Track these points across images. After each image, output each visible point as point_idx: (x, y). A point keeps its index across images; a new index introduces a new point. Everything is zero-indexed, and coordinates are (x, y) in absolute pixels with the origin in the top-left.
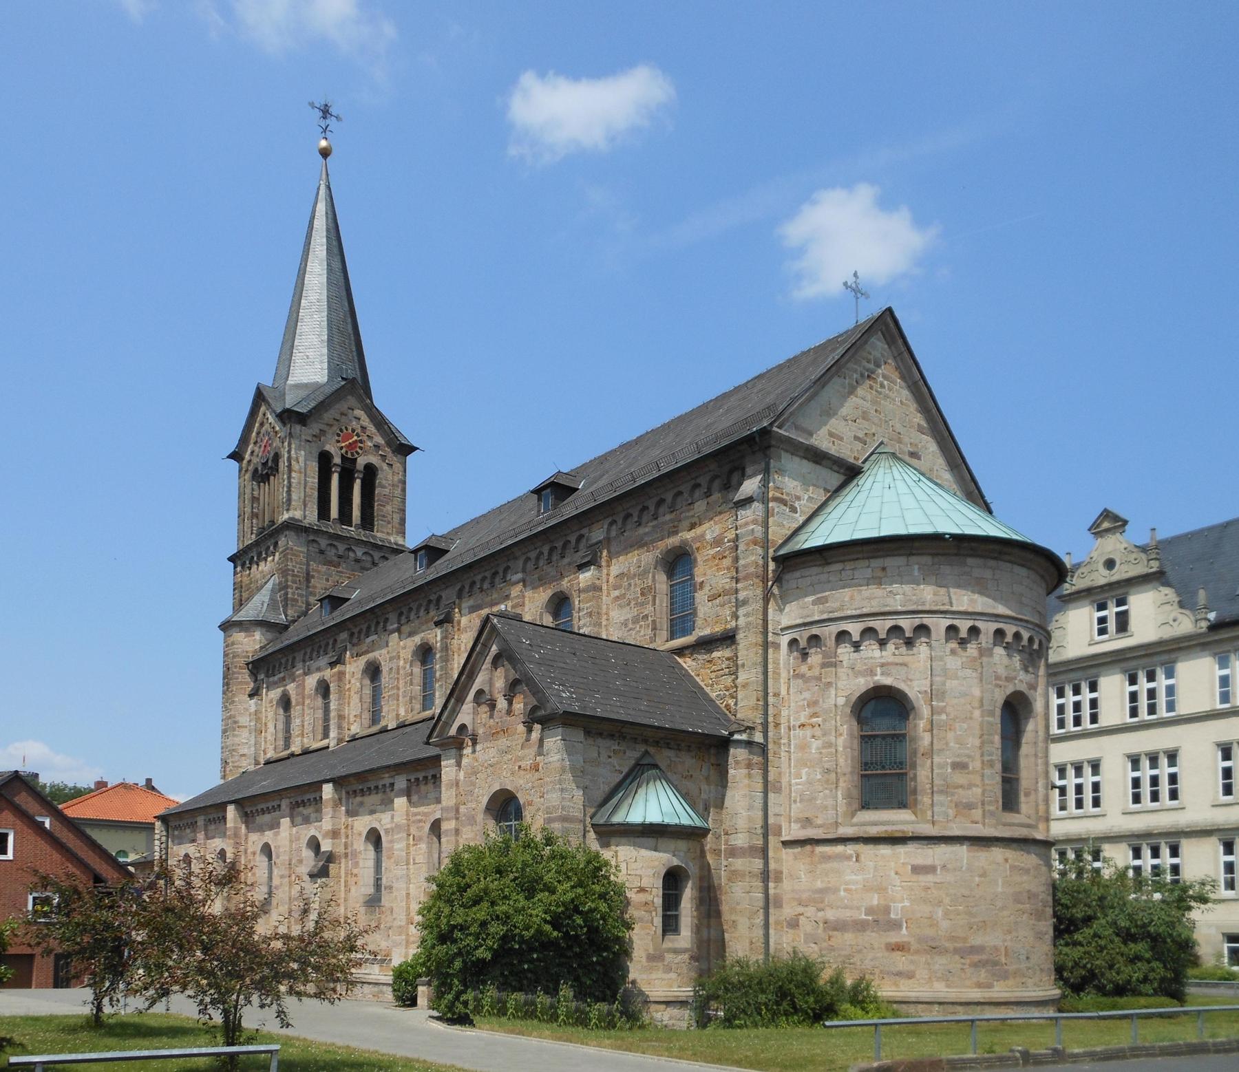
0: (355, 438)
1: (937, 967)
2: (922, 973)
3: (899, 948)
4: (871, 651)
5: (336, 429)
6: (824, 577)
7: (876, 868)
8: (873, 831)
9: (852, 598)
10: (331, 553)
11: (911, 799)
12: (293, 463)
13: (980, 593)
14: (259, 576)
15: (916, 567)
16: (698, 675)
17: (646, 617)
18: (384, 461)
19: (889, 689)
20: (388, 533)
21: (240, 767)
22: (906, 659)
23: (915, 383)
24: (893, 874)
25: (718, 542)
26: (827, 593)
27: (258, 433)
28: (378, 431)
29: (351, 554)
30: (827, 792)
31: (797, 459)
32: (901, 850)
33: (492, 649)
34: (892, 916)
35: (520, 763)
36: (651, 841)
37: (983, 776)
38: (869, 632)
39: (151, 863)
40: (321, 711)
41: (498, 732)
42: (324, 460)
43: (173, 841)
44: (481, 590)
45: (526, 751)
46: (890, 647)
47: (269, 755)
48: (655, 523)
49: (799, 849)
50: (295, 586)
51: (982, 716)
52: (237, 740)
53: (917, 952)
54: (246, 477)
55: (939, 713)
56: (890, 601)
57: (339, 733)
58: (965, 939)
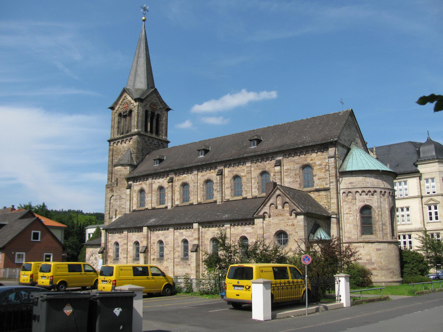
1: (383, 273)
2: (379, 275)
4: (364, 196)
7: (368, 250)
8: (367, 240)
10: (148, 142)
11: (374, 232)
12: (139, 114)
14: (121, 148)
17: (297, 181)
21: (122, 212)
23: (356, 126)
24: (372, 251)
25: (320, 165)
27: (122, 102)
29: (153, 142)
30: (355, 230)
31: (340, 147)
35: (287, 224)
40: (159, 196)
41: (278, 215)
47: (134, 208)
50: (139, 153)
53: (378, 270)
56: (367, 185)
58: (388, 266)
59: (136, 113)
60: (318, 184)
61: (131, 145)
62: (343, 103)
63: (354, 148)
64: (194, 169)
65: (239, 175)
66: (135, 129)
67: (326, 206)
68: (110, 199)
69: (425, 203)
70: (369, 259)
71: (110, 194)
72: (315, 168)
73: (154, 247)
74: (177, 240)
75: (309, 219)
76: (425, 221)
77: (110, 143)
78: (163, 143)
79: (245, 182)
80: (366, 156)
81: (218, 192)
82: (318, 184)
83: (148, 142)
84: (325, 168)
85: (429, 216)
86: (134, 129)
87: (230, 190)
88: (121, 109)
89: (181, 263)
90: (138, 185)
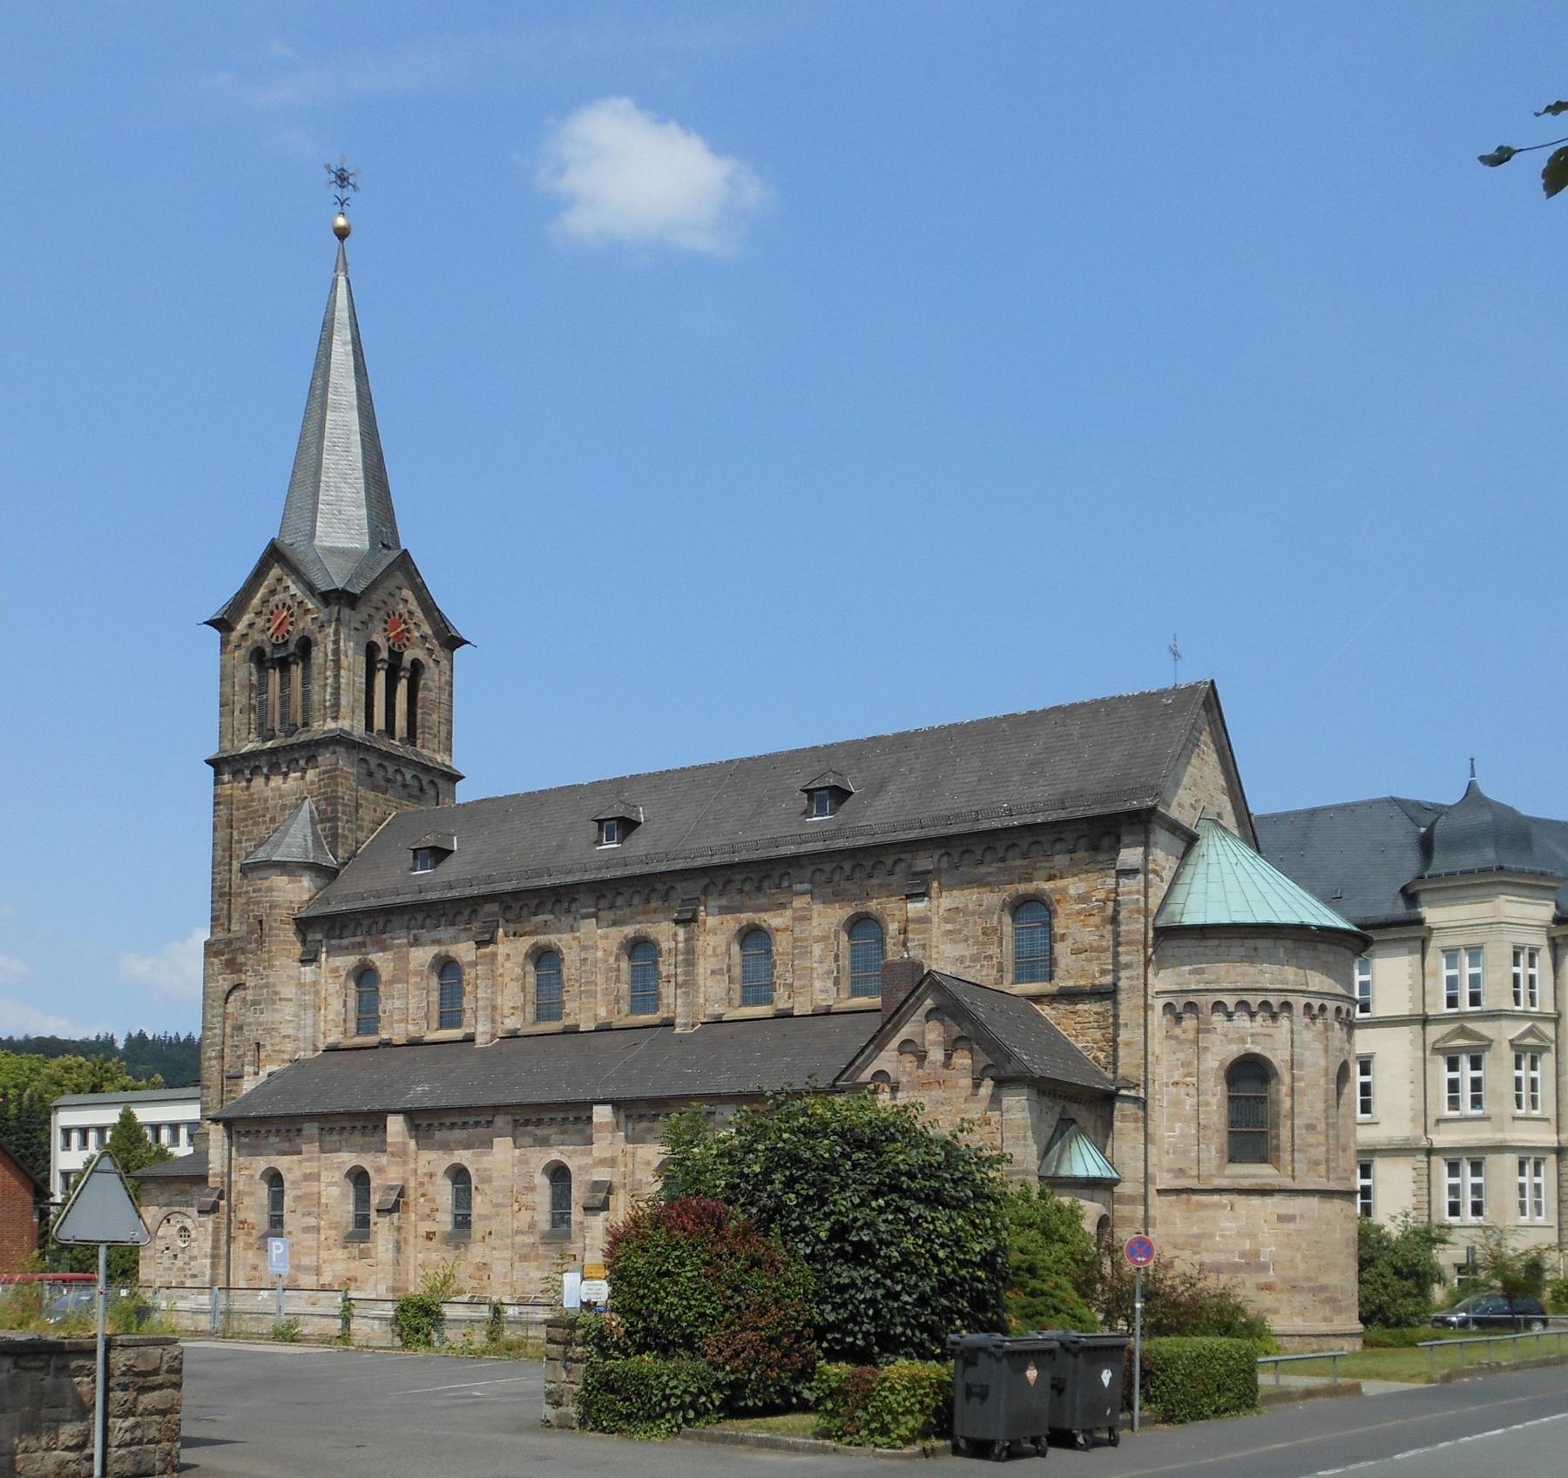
0: (403, 626)
3: (1268, 1287)
4: (1242, 1020)
5: (382, 613)
6: (1200, 950)
8: (1246, 1183)
9: (1227, 972)
10: (380, 774)
13: (1329, 976)
14: (270, 794)
15: (1282, 950)
16: (1059, 1024)
17: (991, 957)
18: (431, 656)
19: (1257, 1055)
20: (434, 750)
21: (283, 1052)
22: (1272, 1031)
23: (1222, 747)
24: (1262, 1222)
25: (1083, 898)
26: (1204, 965)
27: (264, 602)
28: (426, 617)
31: (1163, 831)
32: (1269, 1200)
33: (926, 1003)
34: (1262, 1259)
35: (963, 1116)
36: (1088, 1192)
37: (1327, 1136)
38: (1242, 1004)
39: (202, 1179)
41: (930, 1083)
42: (371, 650)
43: (237, 1151)
44: (741, 891)
45: (972, 1105)
46: (1259, 1018)
47: (331, 1040)
48: (1000, 865)
49: (1174, 1197)
50: (345, 817)
51: (1327, 1084)
52: (277, 1016)
53: (1282, 1291)
54: (236, 655)
55: (1299, 1081)
57: (493, 1028)
59: (330, 654)
60: (1071, 970)
61: (312, 783)
62: (1171, 650)
63: (1210, 836)
64: (582, 895)
65: (764, 925)
66: (329, 720)
67: (1099, 1054)
68: (227, 998)
69: (1434, 1043)
70: (1250, 1250)
71: (224, 980)
72: (1061, 910)
73: (431, 1189)
74: (525, 1166)
75: (1046, 1101)
76: (1429, 1113)
77: (217, 773)
78: (436, 780)
79: (788, 954)
80: (1257, 867)
81: (681, 987)
82: (1071, 970)
83: (380, 774)
84: (1102, 909)
85: (1445, 1094)
86: (325, 721)
87: (724, 981)
88: (263, 631)
89: (541, 1250)
90: (347, 948)
